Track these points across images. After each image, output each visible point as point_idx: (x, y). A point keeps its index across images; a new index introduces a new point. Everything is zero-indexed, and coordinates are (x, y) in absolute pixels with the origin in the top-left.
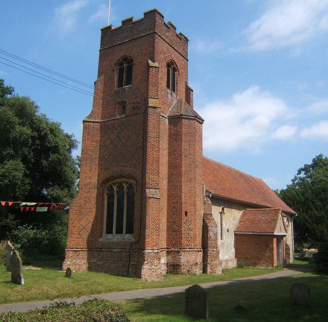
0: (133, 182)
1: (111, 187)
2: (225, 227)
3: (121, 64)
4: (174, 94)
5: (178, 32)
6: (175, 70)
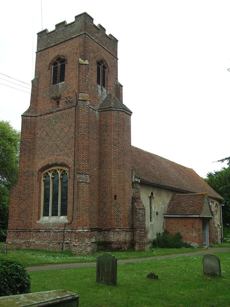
1: (47, 173)
3: (55, 64)
4: (104, 90)
6: (104, 67)
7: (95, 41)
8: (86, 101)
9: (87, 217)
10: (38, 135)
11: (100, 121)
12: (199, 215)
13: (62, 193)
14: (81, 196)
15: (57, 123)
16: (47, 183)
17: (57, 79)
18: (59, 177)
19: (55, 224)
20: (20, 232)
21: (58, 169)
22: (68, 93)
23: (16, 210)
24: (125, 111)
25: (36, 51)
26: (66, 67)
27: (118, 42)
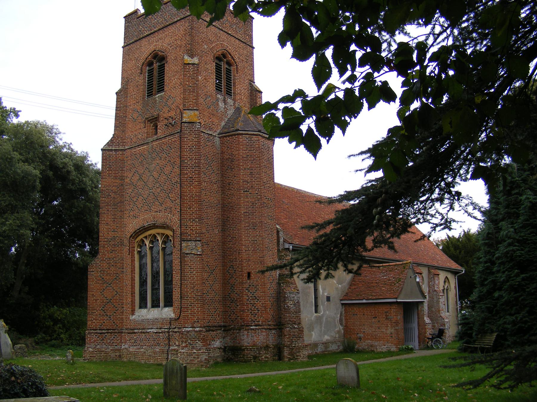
0: (170, 233)
1: (143, 241)
2: (323, 293)
3: (150, 64)
4: (229, 100)
8: (193, 123)
9: (199, 309)
10: (127, 180)
11: (222, 153)
12: (396, 298)
13: (165, 271)
15: (154, 159)
16: (142, 257)
17: (152, 89)
18: (160, 245)
19: (155, 321)
20: (105, 333)
21: (158, 234)
22: (169, 111)
23: (98, 299)
24: (261, 134)
25: (123, 45)
26: (167, 68)
27: (253, 20)
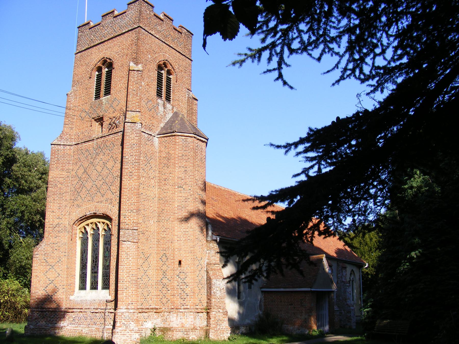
5: (176, 24)
6: (169, 73)
7: (155, 37)
12: (311, 288)
14: (125, 262)
21: (99, 222)
22: (114, 112)
